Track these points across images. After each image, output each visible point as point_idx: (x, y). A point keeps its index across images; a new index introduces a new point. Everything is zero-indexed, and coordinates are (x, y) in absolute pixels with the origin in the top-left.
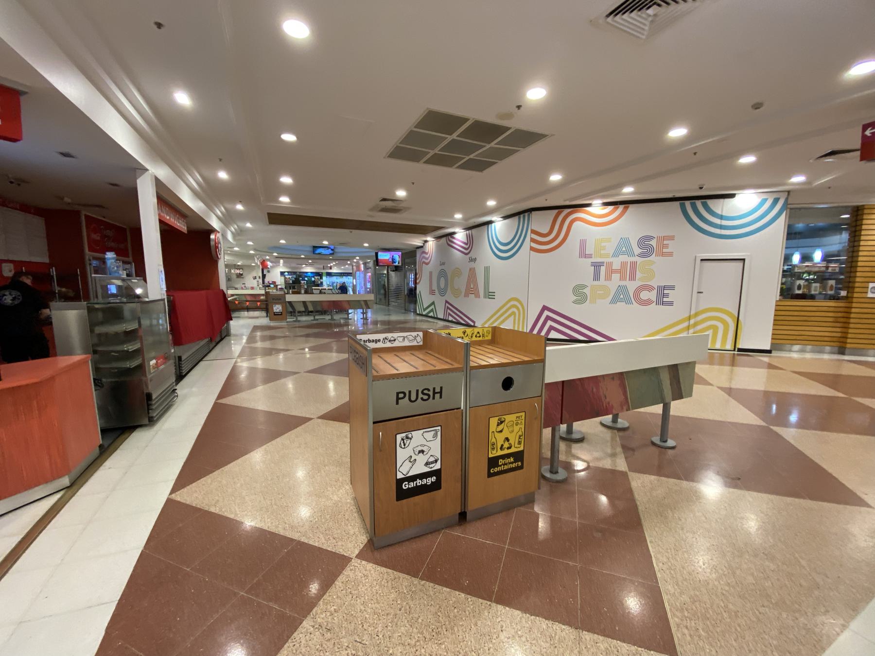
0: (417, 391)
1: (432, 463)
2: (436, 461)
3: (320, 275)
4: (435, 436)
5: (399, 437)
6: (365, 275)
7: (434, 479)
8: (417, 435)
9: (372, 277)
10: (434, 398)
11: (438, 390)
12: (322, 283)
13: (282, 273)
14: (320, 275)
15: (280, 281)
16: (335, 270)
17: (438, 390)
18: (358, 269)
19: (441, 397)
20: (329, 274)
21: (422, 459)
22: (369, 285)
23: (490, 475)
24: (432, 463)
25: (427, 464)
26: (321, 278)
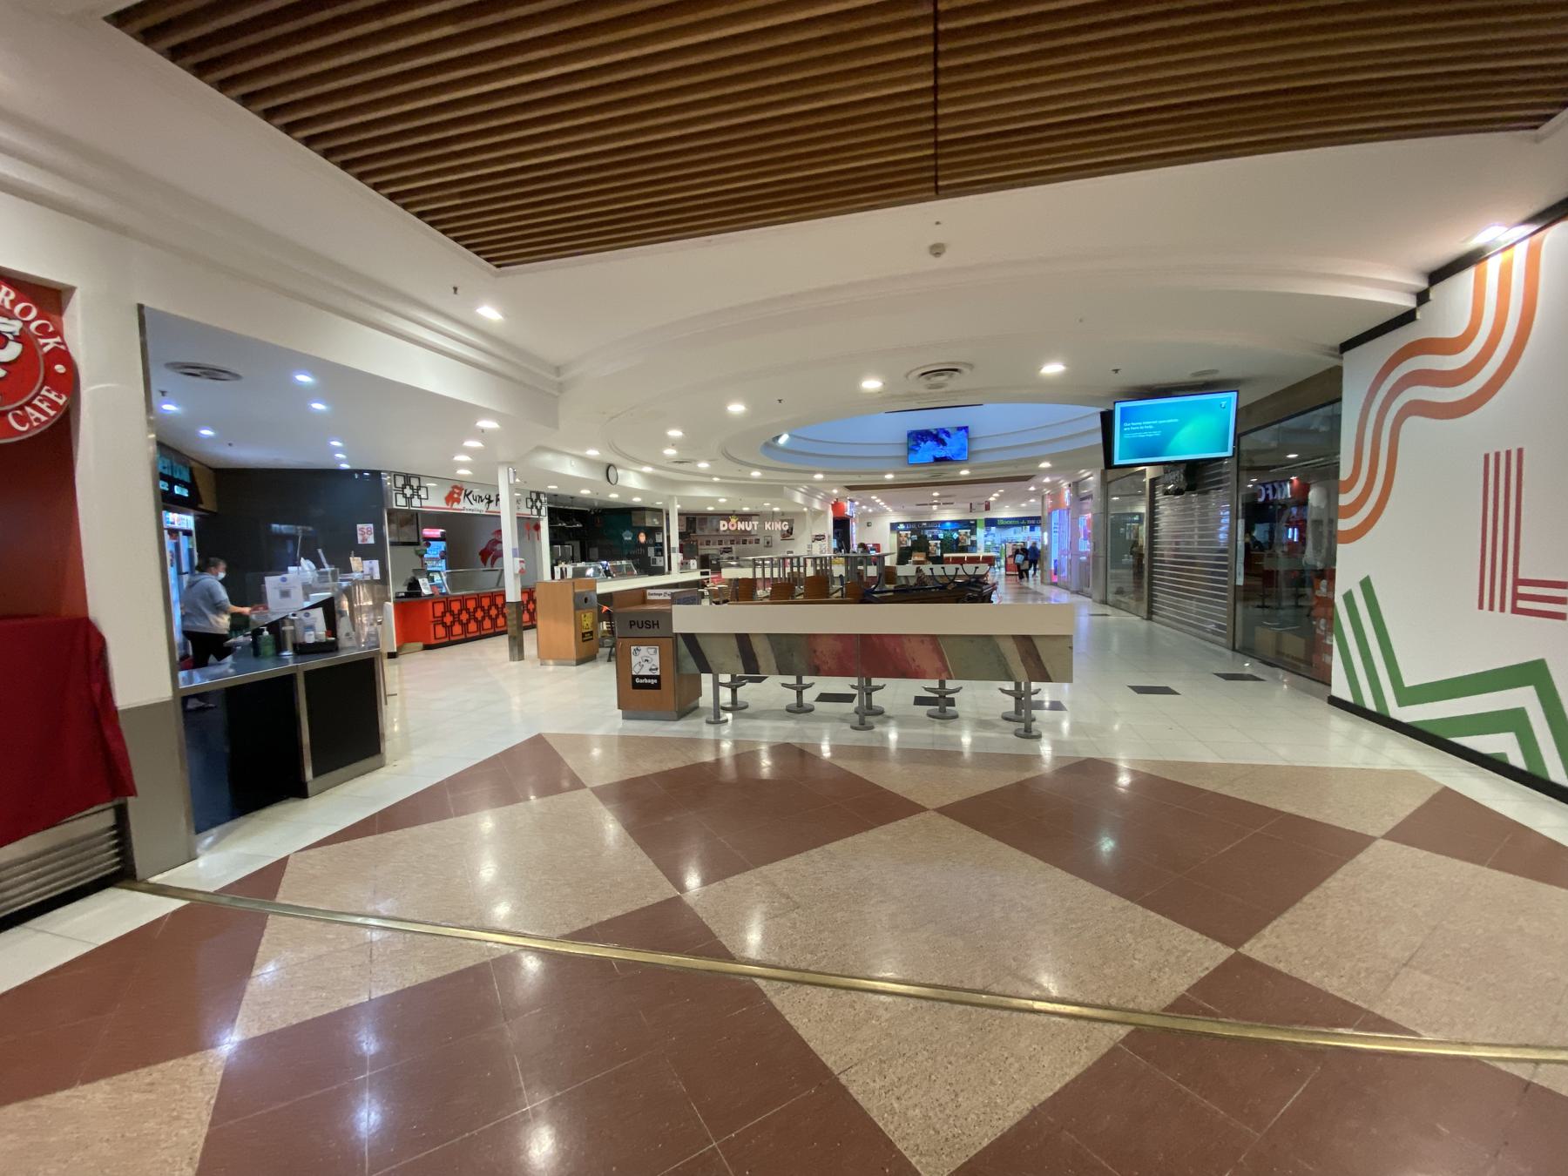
3: (971, 525)
6: (1075, 520)
9: (1094, 524)
12: (974, 543)
13: (894, 527)
14: (971, 525)
15: (889, 544)
16: (1005, 513)
18: (1057, 505)
21: (647, 666)
22: (1085, 546)
26: (973, 533)
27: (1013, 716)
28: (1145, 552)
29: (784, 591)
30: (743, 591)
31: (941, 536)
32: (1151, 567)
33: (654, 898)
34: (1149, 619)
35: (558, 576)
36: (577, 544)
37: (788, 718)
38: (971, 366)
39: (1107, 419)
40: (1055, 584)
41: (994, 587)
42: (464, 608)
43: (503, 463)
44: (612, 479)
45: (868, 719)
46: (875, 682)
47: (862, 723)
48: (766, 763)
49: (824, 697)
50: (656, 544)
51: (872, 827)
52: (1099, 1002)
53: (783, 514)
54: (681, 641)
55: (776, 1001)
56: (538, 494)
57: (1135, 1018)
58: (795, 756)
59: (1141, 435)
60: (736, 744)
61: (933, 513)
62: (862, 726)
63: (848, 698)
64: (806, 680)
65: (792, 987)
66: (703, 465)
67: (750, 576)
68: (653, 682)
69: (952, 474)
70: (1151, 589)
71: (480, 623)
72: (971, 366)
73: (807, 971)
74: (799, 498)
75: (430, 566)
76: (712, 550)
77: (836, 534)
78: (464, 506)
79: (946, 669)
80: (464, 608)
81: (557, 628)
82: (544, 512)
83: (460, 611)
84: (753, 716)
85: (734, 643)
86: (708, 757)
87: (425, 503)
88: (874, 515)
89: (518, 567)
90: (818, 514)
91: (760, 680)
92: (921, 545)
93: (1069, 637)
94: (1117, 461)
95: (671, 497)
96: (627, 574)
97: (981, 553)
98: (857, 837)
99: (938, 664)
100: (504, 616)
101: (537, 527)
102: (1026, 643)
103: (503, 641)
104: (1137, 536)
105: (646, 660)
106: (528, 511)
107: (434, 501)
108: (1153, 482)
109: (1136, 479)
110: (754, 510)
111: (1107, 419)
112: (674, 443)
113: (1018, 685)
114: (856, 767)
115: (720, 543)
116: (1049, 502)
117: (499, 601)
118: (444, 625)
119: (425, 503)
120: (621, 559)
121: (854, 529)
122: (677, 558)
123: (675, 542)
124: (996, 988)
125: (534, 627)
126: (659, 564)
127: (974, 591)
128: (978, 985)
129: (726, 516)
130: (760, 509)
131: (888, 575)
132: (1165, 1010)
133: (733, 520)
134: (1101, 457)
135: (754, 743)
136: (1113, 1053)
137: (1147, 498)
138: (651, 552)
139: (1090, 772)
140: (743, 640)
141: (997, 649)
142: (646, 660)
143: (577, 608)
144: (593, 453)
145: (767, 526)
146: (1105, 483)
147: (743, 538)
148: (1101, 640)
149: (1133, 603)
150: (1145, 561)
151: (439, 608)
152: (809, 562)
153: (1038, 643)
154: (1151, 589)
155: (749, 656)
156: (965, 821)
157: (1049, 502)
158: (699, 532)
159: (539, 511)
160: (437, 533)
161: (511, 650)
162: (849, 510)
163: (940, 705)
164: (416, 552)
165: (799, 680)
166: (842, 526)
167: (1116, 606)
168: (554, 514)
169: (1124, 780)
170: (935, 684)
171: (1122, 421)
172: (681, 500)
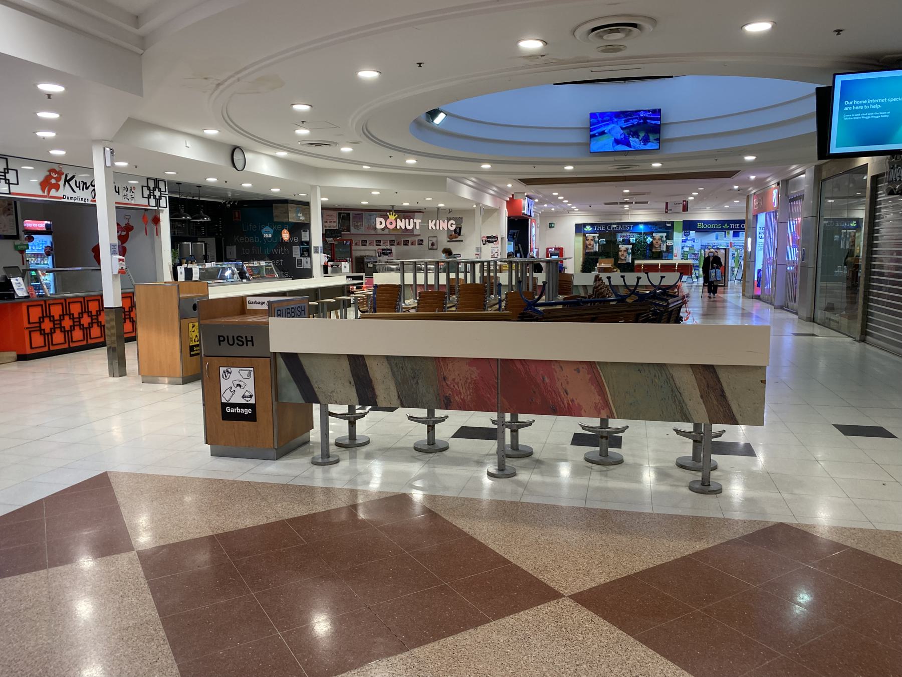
1: (248, 397)
2: (251, 396)
3: (667, 228)
4: (249, 375)
5: (222, 369)
7: (250, 411)
8: (235, 370)
9: (804, 230)
11: (249, 339)
12: (670, 249)
13: (579, 228)
14: (667, 228)
16: (706, 215)
17: (249, 339)
20: (689, 226)
21: (240, 392)
22: (793, 254)
23: (191, 356)
24: (248, 397)
25: (244, 397)
26: (670, 237)
27: (690, 463)
28: (862, 263)
29: (433, 304)
30: (386, 302)
31: (633, 240)
32: (868, 280)
34: (863, 340)
35: (181, 277)
36: (212, 241)
37: (413, 459)
38: (653, 21)
39: (824, 97)
40: (758, 298)
41: (684, 301)
42: (66, 313)
43: (97, 141)
44: (239, 165)
45: (509, 463)
46: (522, 417)
47: (501, 468)
49: (465, 432)
50: (302, 243)
53: (450, 211)
54: (281, 361)
56: (157, 181)
59: (865, 117)
61: (625, 213)
64: (439, 413)
66: (347, 150)
67: (398, 282)
68: (248, 411)
69: (643, 166)
70: (866, 306)
71: (68, 333)
72: (653, 21)
74: (465, 192)
75: (33, 263)
76: (369, 251)
77: (511, 236)
78: (64, 194)
79: (606, 404)
80: (66, 313)
81: (159, 340)
82: (163, 202)
83: (62, 317)
85: (346, 364)
87: (14, 189)
88: (559, 214)
89: (117, 267)
90: (489, 212)
92: (609, 250)
93: (763, 368)
94: (834, 149)
95: (313, 187)
96: (268, 276)
97: (677, 260)
99: (597, 399)
100: (102, 327)
101: (156, 221)
102: (708, 375)
103: (103, 352)
104: (853, 244)
105: (238, 385)
106: (145, 202)
107: (28, 186)
108: (875, 179)
109: (856, 177)
111: (824, 97)
113: (697, 426)
115: (378, 243)
116: (753, 203)
117: (93, 307)
118: (42, 332)
119: (14, 189)
120: (259, 259)
121: (534, 230)
122: (318, 259)
123: (317, 240)
125: (134, 339)
126: (306, 266)
127: (660, 307)
129: (384, 212)
130: (421, 205)
131: (563, 282)
133: (392, 218)
134: (814, 149)
137: (867, 200)
138: (296, 251)
139: (784, 540)
140: (357, 362)
141: (670, 379)
142: (238, 385)
143: (183, 316)
144: (211, 132)
145: (431, 225)
146: (819, 180)
147: (404, 238)
148: (805, 365)
149: (845, 321)
150: (861, 274)
151: (36, 313)
152: (477, 266)
153: (722, 375)
154: (866, 306)
155: (363, 380)
157: (753, 203)
158: (353, 230)
159: (158, 204)
160: (41, 225)
161: (111, 364)
162: (526, 207)
163: (602, 446)
164: (16, 247)
165: (431, 413)
166: (519, 227)
167: (825, 324)
168: (175, 206)
170: (595, 422)
171: (842, 99)
172: (325, 191)
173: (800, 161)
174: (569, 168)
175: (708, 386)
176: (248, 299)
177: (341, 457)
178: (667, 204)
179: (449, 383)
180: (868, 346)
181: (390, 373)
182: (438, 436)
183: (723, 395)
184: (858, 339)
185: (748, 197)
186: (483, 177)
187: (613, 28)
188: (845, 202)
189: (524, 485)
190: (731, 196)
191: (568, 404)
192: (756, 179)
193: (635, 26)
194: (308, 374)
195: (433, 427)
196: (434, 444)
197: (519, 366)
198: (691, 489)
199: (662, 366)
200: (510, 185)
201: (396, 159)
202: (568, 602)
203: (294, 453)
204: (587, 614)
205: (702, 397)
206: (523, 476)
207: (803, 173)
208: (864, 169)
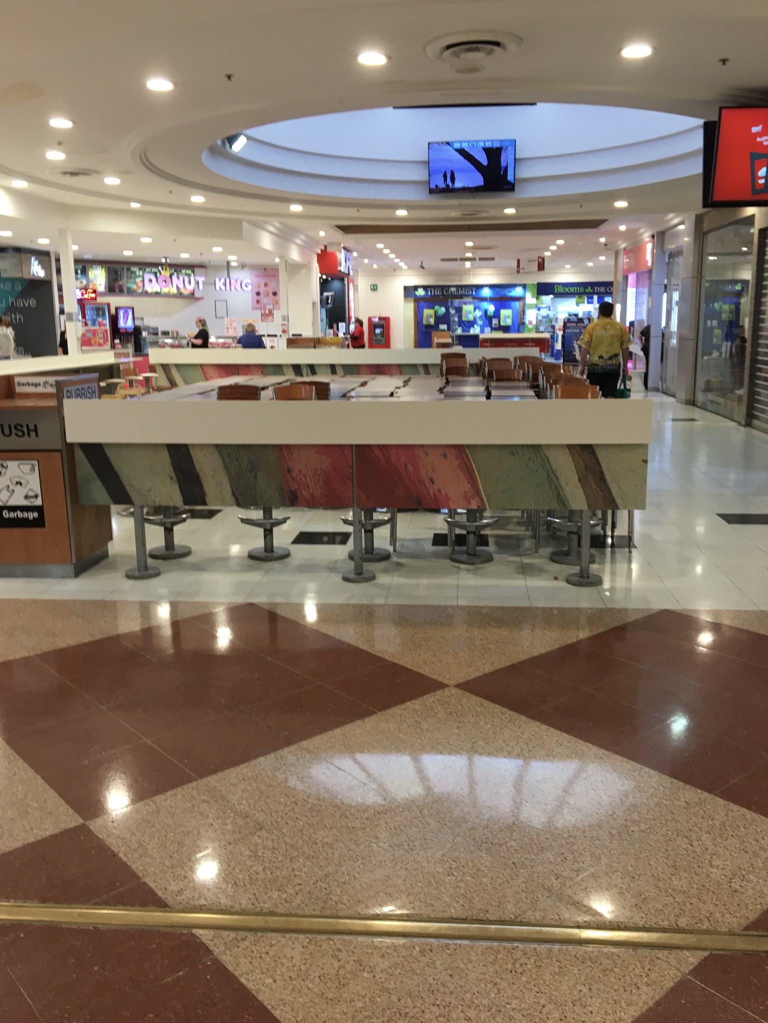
0: (10, 426)
2: (36, 496)
4: (33, 469)
7: (36, 515)
10: (29, 435)
11: (32, 427)
16: (565, 276)
17: (32, 427)
19: (37, 435)
20: (544, 289)
24: (32, 497)
28: (747, 334)
33: (48, 829)
34: (748, 424)
37: (251, 569)
38: (519, 39)
45: (369, 567)
48: (224, 637)
49: (304, 538)
51: (371, 713)
52: (665, 924)
54: (79, 454)
55: (227, 960)
57: (707, 941)
58: (265, 624)
60: (174, 606)
61: (467, 272)
62: (359, 576)
63: (343, 538)
65: (250, 936)
66: (112, 181)
68: (32, 515)
69: (493, 212)
72: (519, 39)
73: (272, 914)
74: (266, 241)
84: (199, 567)
85: (165, 456)
86: (129, 625)
91: (211, 514)
93: (644, 447)
98: (347, 728)
99: (467, 487)
109: (743, 229)
110: (197, 259)
112: (60, 140)
114: (349, 634)
124: (530, 916)
128: (510, 910)
132: (747, 928)
135: (207, 605)
136: (681, 988)
146: (700, 233)
150: (748, 345)
156: (470, 691)
165: (268, 513)
169: (706, 638)
173: (678, 210)
174: (402, 213)
175: (586, 469)
176: (17, 380)
177: (162, 570)
178: (519, 261)
179: (294, 475)
180: (754, 432)
181: (222, 466)
182: (276, 543)
183: (602, 478)
184: (743, 423)
185: (617, 253)
186: (291, 222)
187: (472, 45)
188: (729, 260)
189: (388, 588)
190: (596, 251)
191: (435, 494)
192: (628, 231)
193: (497, 44)
194: (117, 469)
195: (271, 531)
196: (272, 551)
197: (377, 452)
198: (568, 582)
199: (536, 448)
200: (322, 234)
201: (178, 194)
202: (454, 691)
203: (98, 567)
204: (475, 700)
205: (580, 481)
206: (383, 579)
207: (682, 223)
208: (751, 220)
